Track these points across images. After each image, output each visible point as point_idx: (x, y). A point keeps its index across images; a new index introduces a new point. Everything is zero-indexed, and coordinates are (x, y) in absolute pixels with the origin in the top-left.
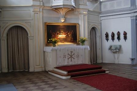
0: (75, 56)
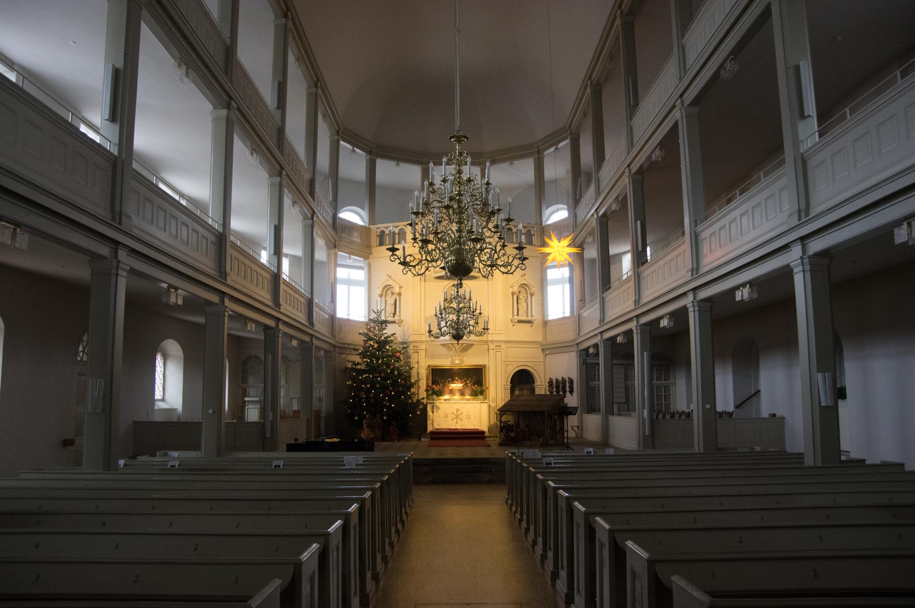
0: (463, 416)
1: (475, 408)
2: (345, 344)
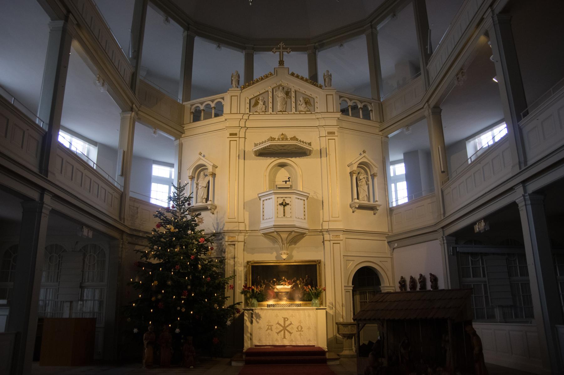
1: (309, 316)
2: (140, 231)
